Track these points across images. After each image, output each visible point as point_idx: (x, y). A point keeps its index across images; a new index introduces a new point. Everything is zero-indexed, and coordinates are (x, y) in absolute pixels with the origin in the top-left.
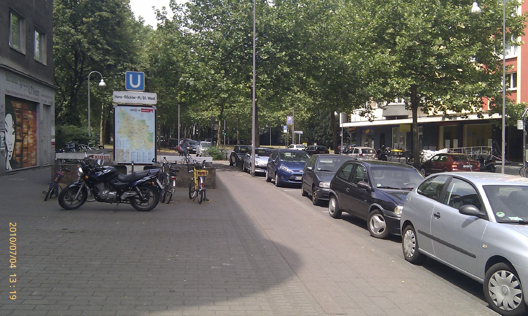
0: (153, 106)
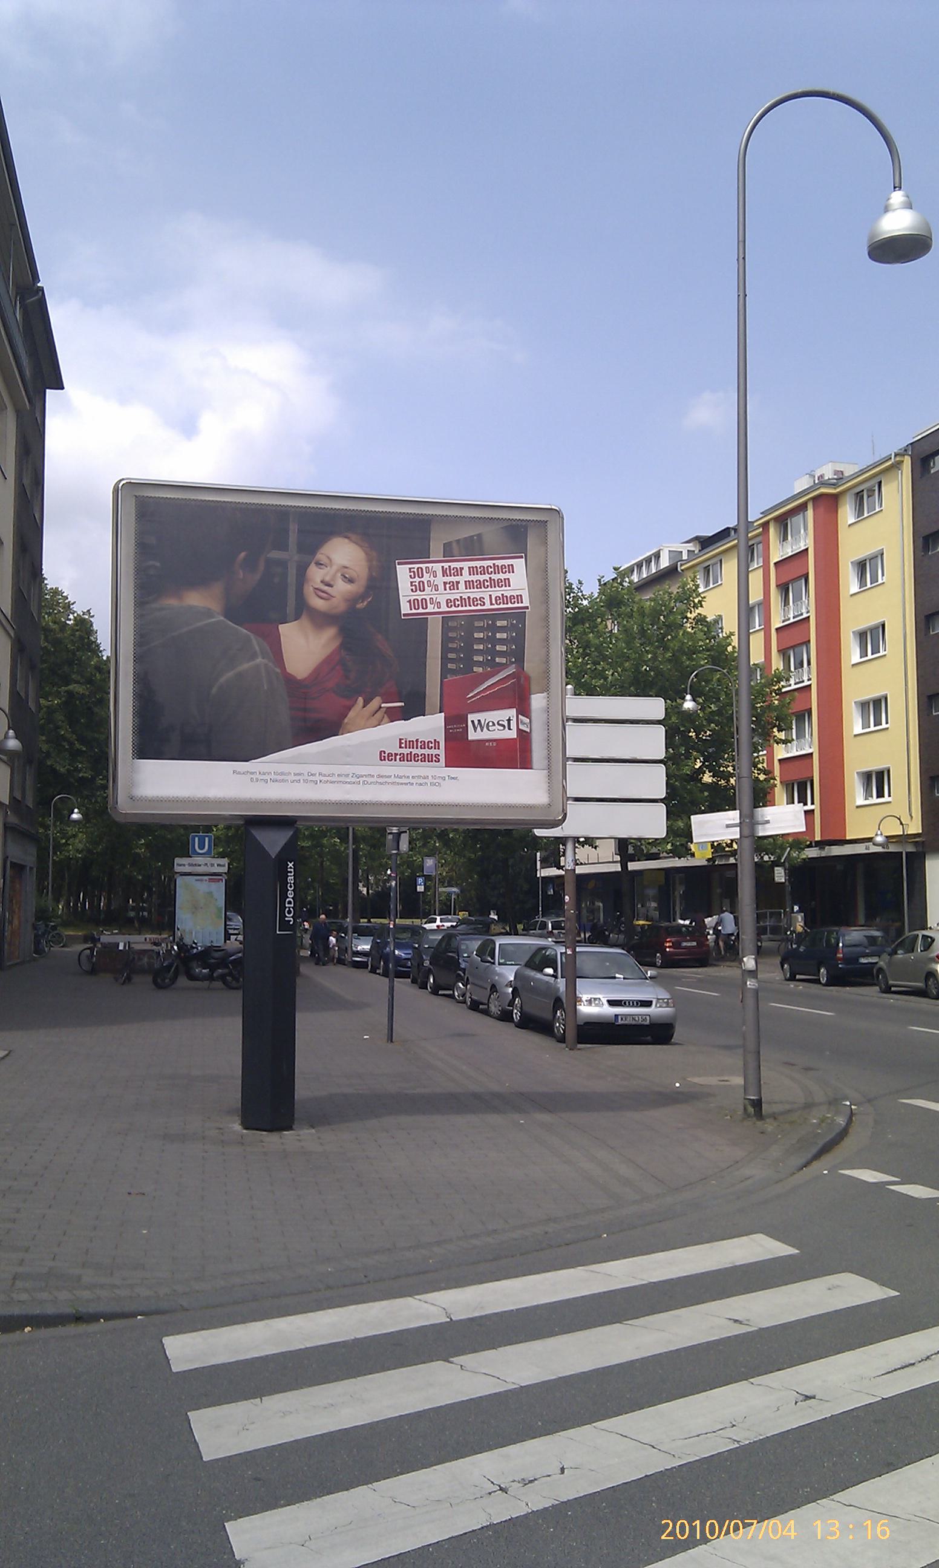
0: (223, 875)
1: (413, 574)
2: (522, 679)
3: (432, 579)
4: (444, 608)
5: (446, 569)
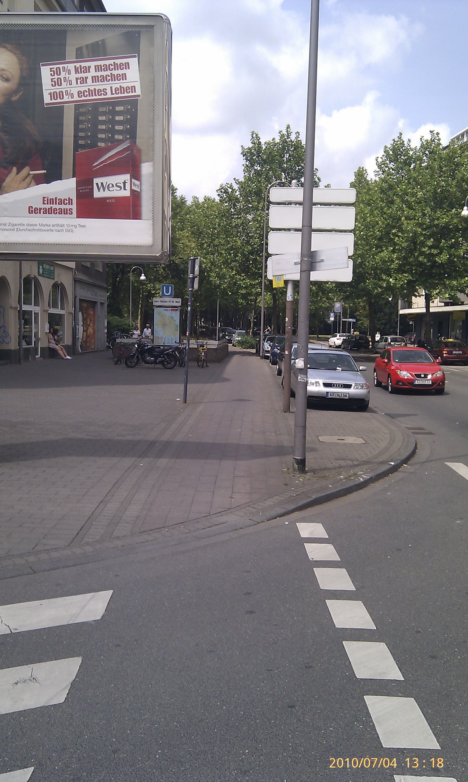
0: (179, 307)
1: (54, 72)
2: (135, 151)
3: (67, 76)
4: (76, 98)
5: (78, 67)
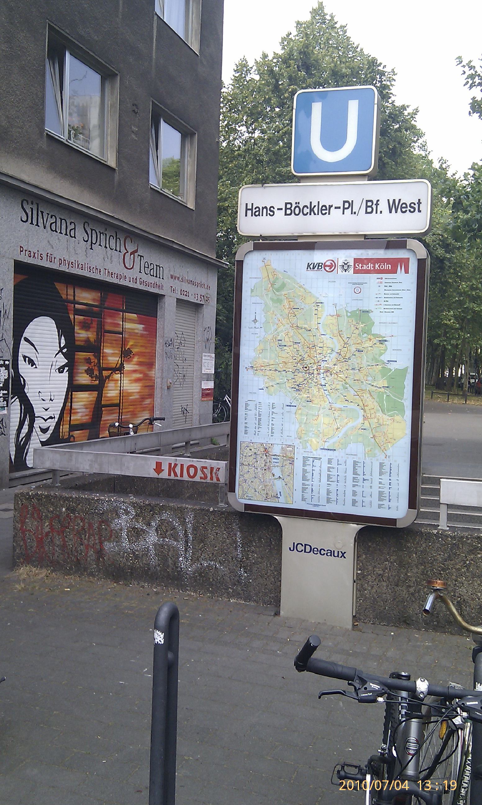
0: (413, 244)
